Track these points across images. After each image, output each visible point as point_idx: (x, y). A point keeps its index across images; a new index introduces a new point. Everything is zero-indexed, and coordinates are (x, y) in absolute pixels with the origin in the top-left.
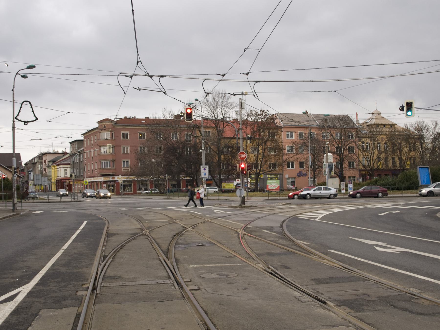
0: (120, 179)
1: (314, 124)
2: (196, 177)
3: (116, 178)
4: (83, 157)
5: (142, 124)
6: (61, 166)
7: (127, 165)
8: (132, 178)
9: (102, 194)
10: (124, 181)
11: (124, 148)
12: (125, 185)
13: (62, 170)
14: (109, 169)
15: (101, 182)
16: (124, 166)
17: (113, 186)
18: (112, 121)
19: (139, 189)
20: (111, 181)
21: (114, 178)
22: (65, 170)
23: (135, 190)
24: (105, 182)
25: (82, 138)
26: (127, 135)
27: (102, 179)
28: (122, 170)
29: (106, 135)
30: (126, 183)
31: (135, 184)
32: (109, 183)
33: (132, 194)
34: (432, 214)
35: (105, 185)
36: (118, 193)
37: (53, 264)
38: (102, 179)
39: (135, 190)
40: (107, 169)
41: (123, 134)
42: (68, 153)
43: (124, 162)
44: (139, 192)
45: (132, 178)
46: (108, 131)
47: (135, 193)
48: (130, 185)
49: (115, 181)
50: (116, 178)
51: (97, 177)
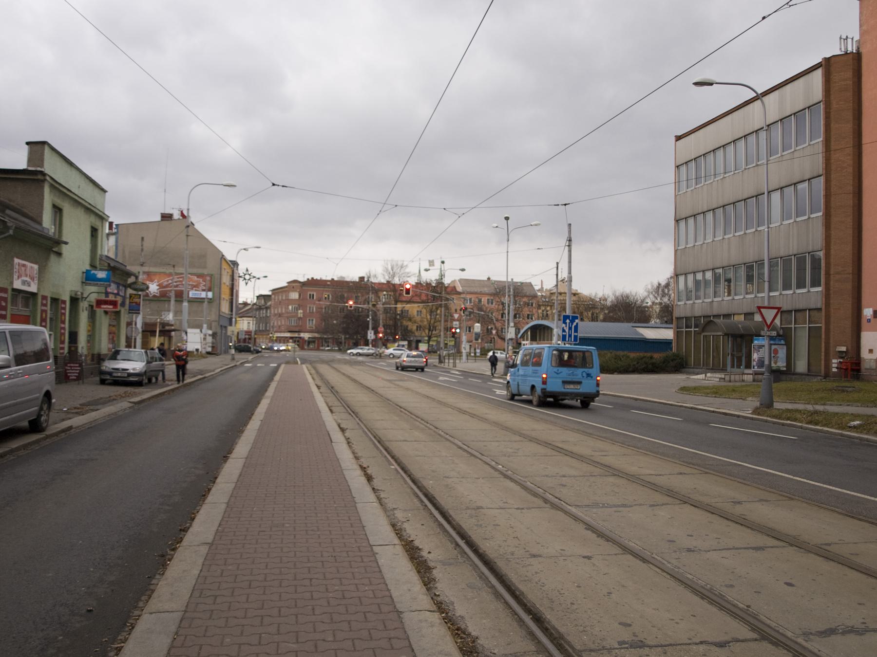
0: (306, 336)
1: (486, 290)
2: (550, 397)
3: (302, 335)
4: (270, 313)
5: (328, 285)
6: (245, 319)
7: (313, 323)
8: (316, 335)
9: (276, 348)
10: (309, 338)
11: (310, 308)
12: (310, 342)
13: (246, 322)
14: (296, 326)
15: (287, 337)
16: (309, 324)
17: (298, 341)
18: (300, 282)
19: (322, 346)
20: (296, 337)
21: (299, 335)
22: (455, 367)
23: (318, 347)
24: (291, 338)
25: (270, 293)
26: (313, 295)
27: (288, 335)
28: (308, 328)
29: (294, 295)
30: (311, 339)
31: (318, 341)
32: (294, 339)
33: (316, 350)
34: (868, 424)
35: (291, 341)
36: (302, 348)
37: (260, 405)
38: (288, 335)
39: (318, 347)
40: (294, 326)
41: (310, 295)
42: (250, 304)
43: (309, 320)
44: (321, 348)
45: (316, 335)
46: (296, 291)
47: (318, 349)
48: (314, 342)
49: (300, 338)
50: (302, 335)
51: (284, 332)
